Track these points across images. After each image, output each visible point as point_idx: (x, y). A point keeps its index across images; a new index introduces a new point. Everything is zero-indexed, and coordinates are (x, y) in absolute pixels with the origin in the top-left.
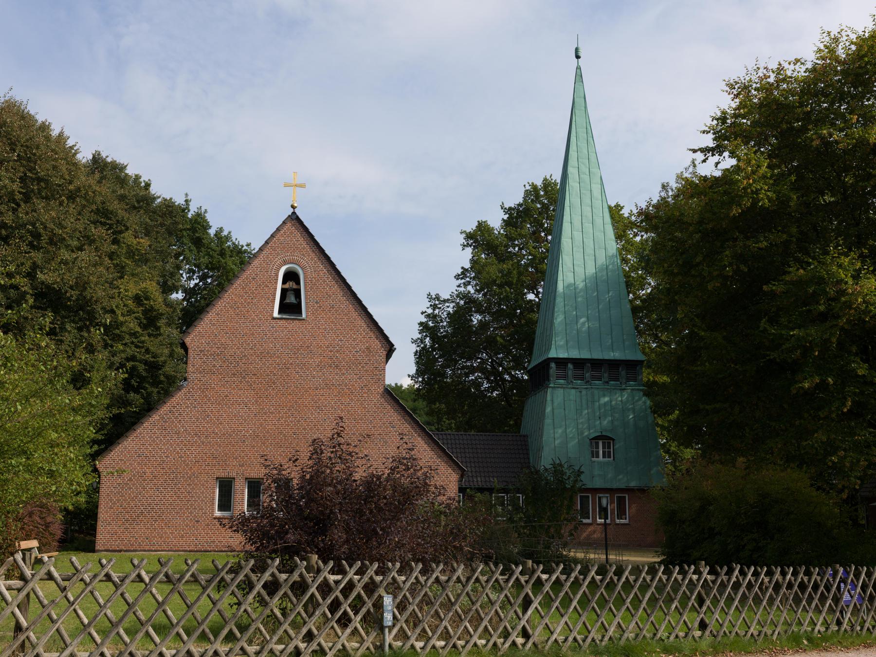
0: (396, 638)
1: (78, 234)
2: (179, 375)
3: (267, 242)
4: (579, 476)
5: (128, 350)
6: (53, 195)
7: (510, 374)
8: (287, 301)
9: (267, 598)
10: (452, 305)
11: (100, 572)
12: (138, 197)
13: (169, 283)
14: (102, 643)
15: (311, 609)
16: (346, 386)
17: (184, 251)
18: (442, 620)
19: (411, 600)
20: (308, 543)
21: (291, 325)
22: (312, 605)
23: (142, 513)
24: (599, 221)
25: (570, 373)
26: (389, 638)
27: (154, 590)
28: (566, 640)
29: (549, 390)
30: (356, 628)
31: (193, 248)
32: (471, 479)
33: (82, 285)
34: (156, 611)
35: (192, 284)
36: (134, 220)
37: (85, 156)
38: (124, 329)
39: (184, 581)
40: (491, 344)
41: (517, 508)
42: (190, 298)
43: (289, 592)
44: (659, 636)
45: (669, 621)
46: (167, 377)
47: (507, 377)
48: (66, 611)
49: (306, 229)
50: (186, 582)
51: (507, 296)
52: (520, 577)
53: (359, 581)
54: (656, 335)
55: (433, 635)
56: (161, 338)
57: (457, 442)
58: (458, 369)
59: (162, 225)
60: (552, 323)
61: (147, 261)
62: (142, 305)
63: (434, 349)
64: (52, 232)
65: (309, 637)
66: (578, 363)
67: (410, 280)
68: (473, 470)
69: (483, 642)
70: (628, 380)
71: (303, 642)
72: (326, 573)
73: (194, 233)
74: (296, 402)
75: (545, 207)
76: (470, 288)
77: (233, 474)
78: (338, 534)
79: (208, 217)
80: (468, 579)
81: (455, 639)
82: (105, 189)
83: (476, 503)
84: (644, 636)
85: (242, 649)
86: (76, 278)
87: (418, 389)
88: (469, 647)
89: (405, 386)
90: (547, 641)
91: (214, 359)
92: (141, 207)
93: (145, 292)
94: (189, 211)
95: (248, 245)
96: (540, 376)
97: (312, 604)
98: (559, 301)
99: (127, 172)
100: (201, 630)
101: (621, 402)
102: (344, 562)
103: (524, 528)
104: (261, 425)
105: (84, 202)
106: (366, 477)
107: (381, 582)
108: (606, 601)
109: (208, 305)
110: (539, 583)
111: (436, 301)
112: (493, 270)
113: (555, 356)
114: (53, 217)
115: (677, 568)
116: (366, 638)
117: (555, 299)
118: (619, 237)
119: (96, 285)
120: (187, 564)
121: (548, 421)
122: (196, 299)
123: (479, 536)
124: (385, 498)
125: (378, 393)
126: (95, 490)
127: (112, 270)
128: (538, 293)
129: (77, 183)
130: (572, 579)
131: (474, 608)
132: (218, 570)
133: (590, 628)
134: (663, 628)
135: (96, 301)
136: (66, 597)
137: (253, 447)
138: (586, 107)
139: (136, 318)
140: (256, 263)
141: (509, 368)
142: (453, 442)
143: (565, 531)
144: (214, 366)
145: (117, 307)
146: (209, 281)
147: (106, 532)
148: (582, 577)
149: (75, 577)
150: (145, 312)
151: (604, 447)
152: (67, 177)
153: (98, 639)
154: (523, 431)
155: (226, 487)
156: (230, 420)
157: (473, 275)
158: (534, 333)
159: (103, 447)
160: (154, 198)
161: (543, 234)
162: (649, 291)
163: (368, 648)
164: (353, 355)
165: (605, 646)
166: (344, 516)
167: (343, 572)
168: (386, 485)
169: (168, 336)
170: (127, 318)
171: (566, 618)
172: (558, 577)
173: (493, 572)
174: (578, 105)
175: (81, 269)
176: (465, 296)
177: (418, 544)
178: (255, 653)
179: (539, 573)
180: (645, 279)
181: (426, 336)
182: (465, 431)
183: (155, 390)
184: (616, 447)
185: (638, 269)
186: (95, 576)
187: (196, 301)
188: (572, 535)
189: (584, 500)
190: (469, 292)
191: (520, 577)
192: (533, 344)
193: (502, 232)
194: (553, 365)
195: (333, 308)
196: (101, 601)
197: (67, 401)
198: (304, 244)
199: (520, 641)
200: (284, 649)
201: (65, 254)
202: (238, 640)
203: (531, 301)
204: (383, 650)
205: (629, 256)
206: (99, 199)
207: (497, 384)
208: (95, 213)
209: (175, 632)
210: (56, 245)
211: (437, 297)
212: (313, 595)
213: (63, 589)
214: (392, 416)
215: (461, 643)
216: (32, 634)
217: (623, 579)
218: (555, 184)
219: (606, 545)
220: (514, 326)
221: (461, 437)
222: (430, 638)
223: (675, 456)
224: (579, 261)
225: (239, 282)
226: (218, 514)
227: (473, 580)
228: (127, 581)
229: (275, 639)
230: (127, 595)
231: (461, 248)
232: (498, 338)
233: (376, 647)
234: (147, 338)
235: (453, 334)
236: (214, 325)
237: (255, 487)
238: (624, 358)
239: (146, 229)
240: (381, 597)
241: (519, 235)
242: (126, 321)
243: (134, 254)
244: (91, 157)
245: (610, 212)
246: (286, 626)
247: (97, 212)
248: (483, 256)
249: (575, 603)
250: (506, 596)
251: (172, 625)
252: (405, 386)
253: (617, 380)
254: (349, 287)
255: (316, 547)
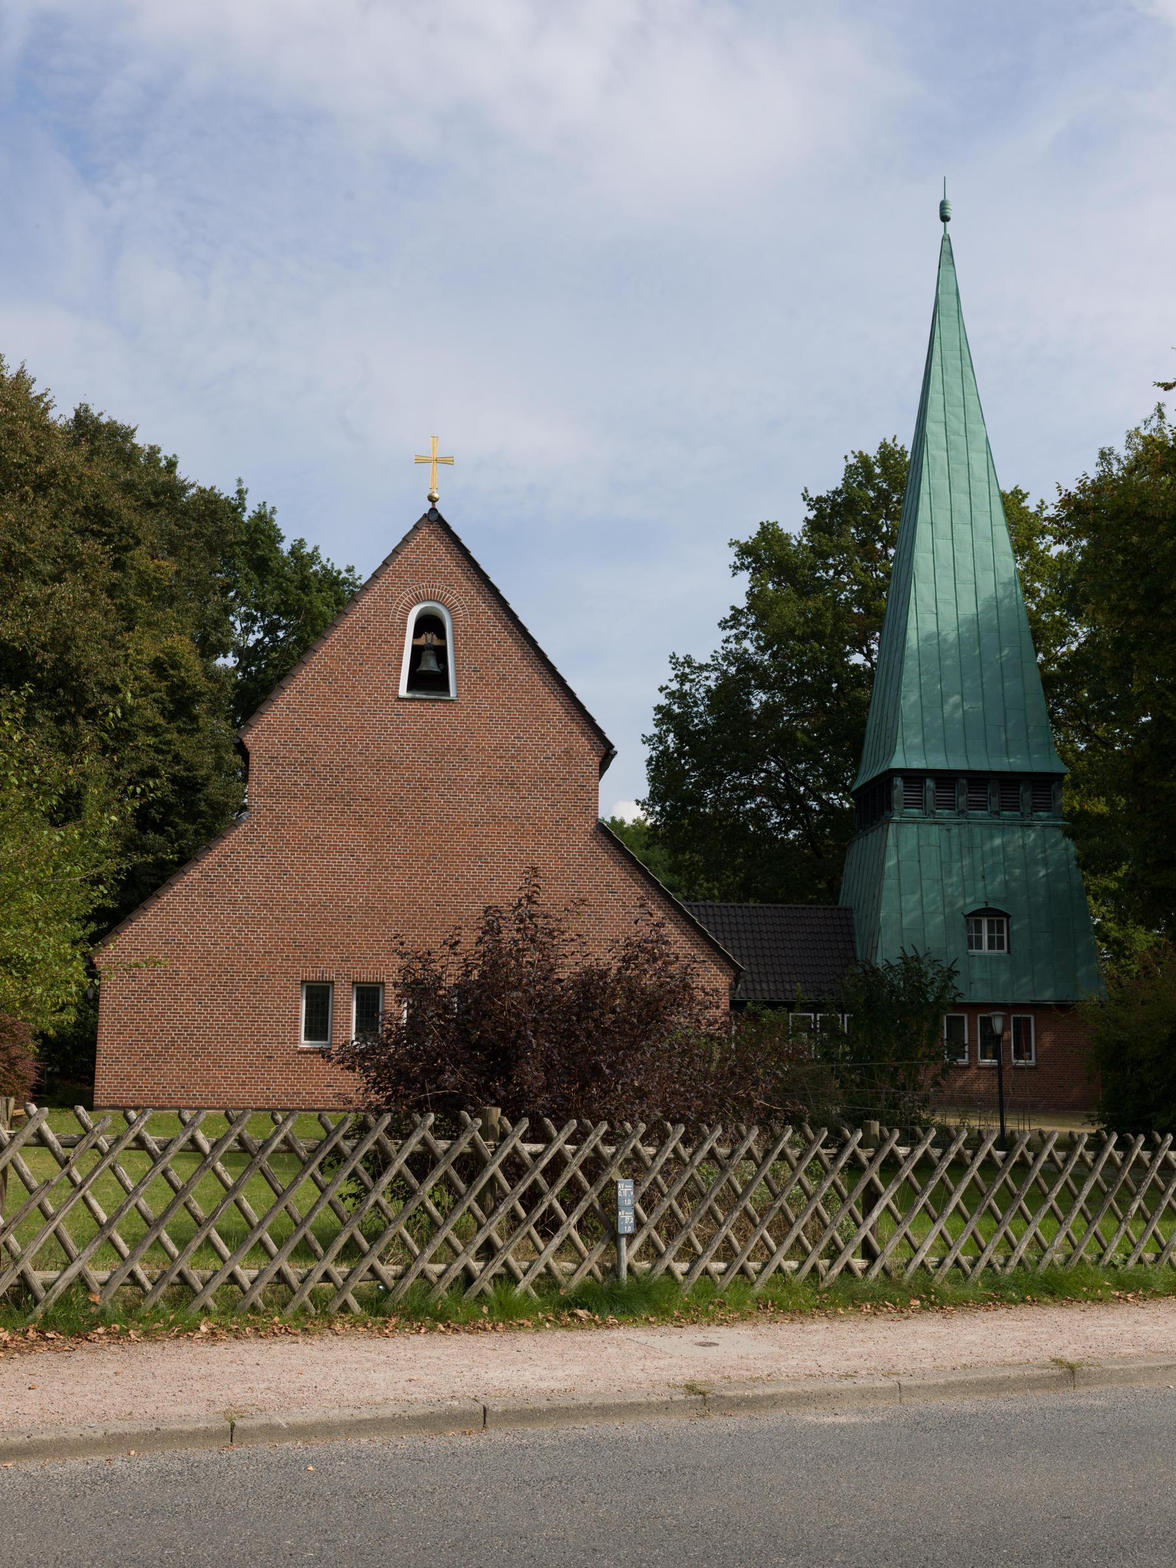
0: (639, 1255)
1: (52, 552)
2: (231, 802)
3: (386, 563)
4: (950, 978)
5: (143, 757)
6: (8, 484)
7: (818, 799)
8: (423, 668)
9: (414, 1181)
10: (714, 675)
11: (126, 1132)
12: (156, 484)
13: (213, 639)
14: (132, 1256)
15: (490, 1203)
16: (528, 818)
17: (236, 581)
18: (720, 1226)
19: (665, 1190)
20: (478, 1090)
21: (431, 712)
22: (492, 1195)
23: (173, 1042)
24: (983, 520)
25: (929, 795)
26: (627, 1255)
27: (219, 1166)
28: (941, 1263)
29: (892, 827)
30: (569, 1237)
31: (253, 575)
32: (750, 986)
33: (62, 642)
34: (223, 1202)
35: (251, 640)
36: (149, 527)
37: (61, 414)
38: (136, 720)
39: (270, 1151)
40: (784, 745)
41: (837, 1035)
42: (249, 666)
43: (453, 1173)
44: (1107, 1258)
45: (1127, 1233)
46: (211, 805)
47: (814, 804)
48: (70, 1199)
49: (455, 540)
50: (274, 1152)
51: (815, 659)
52: (859, 1150)
53: (574, 1155)
54: (1088, 728)
55: (704, 1252)
56: (199, 736)
57: (726, 920)
58: (726, 790)
59: (198, 535)
60: (897, 707)
61: (172, 600)
62: (165, 678)
63: (682, 755)
64: (9, 548)
65: (488, 1250)
66: (945, 779)
67: (639, 630)
68: (755, 969)
69: (794, 1264)
70: (1035, 808)
71: (477, 1260)
72: (516, 1141)
73: (252, 549)
74: (440, 847)
75: (884, 496)
76: (746, 644)
77: (331, 975)
78: (531, 1073)
79: (279, 521)
80: (767, 1153)
81: (744, 1259)
82: (99, 472)
83: (763, 1026)
84: (1081, 1259)
85: (372, 1269)
86: (53, 630)
87: (654, 826)
88: (769, 1272)
89: (629, 822)
90: (907, 1265)
91: (296, 773)
92: (161, 504)
93: (171, 654)
94: (244, 510)
95: (350, 570)
96: (875, 802)
97: (493, 1194)
98: (910, 664)
99: (135, 441)
100: (300, 1236)
101: (1025, 850)
102: (547, 1121)
103: (850, 1071)
104: (379, 887)
105: (63, 496)
106: (580, 975)
107: (613, 1156)
108: (1013, 1196)
109: (281, 677)
110: (891, 1166)
111: (685, 668)
112: (790, 612)
113: (902, 766)
114: (10, 524)
115: (1142, 1139)
116: (587, 1254)
117: (902, 662)
118: (1020, 549)
119: (86, 641)
120: (276, 1122)
121: (889, 883)
122: (259, 667)
123: (780, 1080)
124: (613, 1011)
125: (586, 831)
126: (90, 1002)
127: (113, 615)
128: (871, 652)
129: (50, 462)
130: (952, 1157)
131: (778, 1205)
132: (328, 1131)
133: (984, 1243)
134: (1116, 1244)
135: (87, 671)
136: (68, 1175)
137: (366, 927)
138: (959, 311)
139: (156, 701)
140: (366, 600)
141: (819, 789)
142: (718, 919)
143: (925, 1078)
144: (296, 784)
145: (122, 681)
146: (281, 634)
147: (110, 1074)
148: (969, 1152)
149: (84, 1142)
150: (172, 690)
151: (990, 930)
152: (33, 451)
153: (126, 1250)
154: (843, 902)
155: (319, 998)
156: (332, 875)
157: (752, 620)
158: (864, 724)
159: (105, 925)
160: (184, 489)
161: (879, 546)
162: (1073, 647)
163: (591, 1273)
164: (541, 765)
165: (1012, 1275)
166: (542, 1041)
167: (548, 1140)
168: (614, 989)
169: (212, 732)
170: (141, 701)
171: (941, 1225)
172: (926, 1152)
173: (810, 1142)
174: (945, 309)
175: (59, 613)
176: (739, 659)
177: (674, 1093)
178: (394, 1278)
179: (892, 1144)
180: (1067, 625)
181: (668, 731)
182: (740, 900)
183: (191, 828)
184: (1014, 928)
185: (1054, 608)
186: (118, 1140)
187: (259, 670)
188: (937, 1083)
189: (955, 1023)
190: (746, 651)
191: (859, 1150)
192: (862, 744)
193: (805, 542)
194: (898, 782)
195: (505, 679)
196: (129, 1183)
197: (58, 839)
198: (452, 565)
199: (859, 1263)
200: (445, 1271)
201: (31, 589)
202: (364, 1255)
203: (857, 666)
204: (617, 1276)
205: (1037, 585)
206: (88, 490)
207: (797, 817)
208: (82, 515)
209: (256, 1239)
210: (15, 571)
211: (688, 662)
212: (493, 1178)
213: (64, 1163)
214: (612, 872)
215: (753, 1266)
216: (12, 1239)
217: (1044, 1157)
218: (903, 454)
219: (1001, 1106)
220: (827, 711)
221: (732, 912)
222: (699, 1257)
223: (1119, 948)
224: (946, 593)
225: (337, 634)
226: (305, 1044)
227: (775, 1156)
228: (174, 1150)
229: (429, 1253)
230: (172, 1174)
231: (730, 571)
232: (799, 735)
233: (605, 1271)
234: (176, 735)
235: (717, 728)
236: (294, 711)
237: (368, 996)
238: (1027, 769)
239: (170, 542)
240: (613, 1184)
241: (836, 546)
242: (139, 707)
243: (150, 588)
244: (72, 415)
245: (1004, 504)
246: (447, 1232)
247: (86, 512)
248: (770, 586)
249: (956, 1198)
250: (834, 1184)
251: (252, 1227)
252: (629, 822)
253: (1015, 808)
254: (532, 642)
255: (493, 1096)
